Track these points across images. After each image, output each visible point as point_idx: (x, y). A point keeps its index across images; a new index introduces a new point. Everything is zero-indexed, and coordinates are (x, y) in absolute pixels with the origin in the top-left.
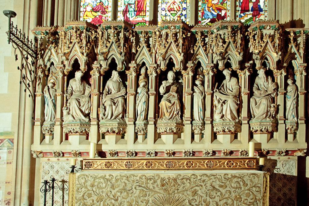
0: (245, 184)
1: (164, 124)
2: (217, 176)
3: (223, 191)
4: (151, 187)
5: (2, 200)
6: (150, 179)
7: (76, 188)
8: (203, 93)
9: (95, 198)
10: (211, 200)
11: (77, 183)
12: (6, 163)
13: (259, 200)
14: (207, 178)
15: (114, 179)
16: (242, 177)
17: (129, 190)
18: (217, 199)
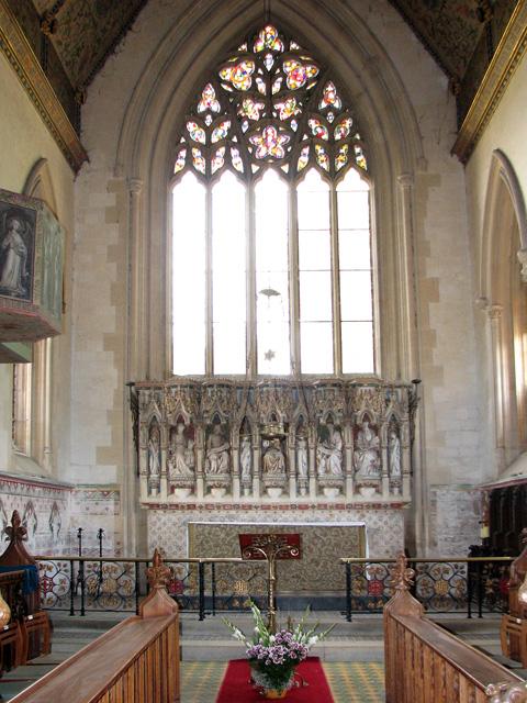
3: (325, 539)
8: (307, 448)
18: (319, 546)
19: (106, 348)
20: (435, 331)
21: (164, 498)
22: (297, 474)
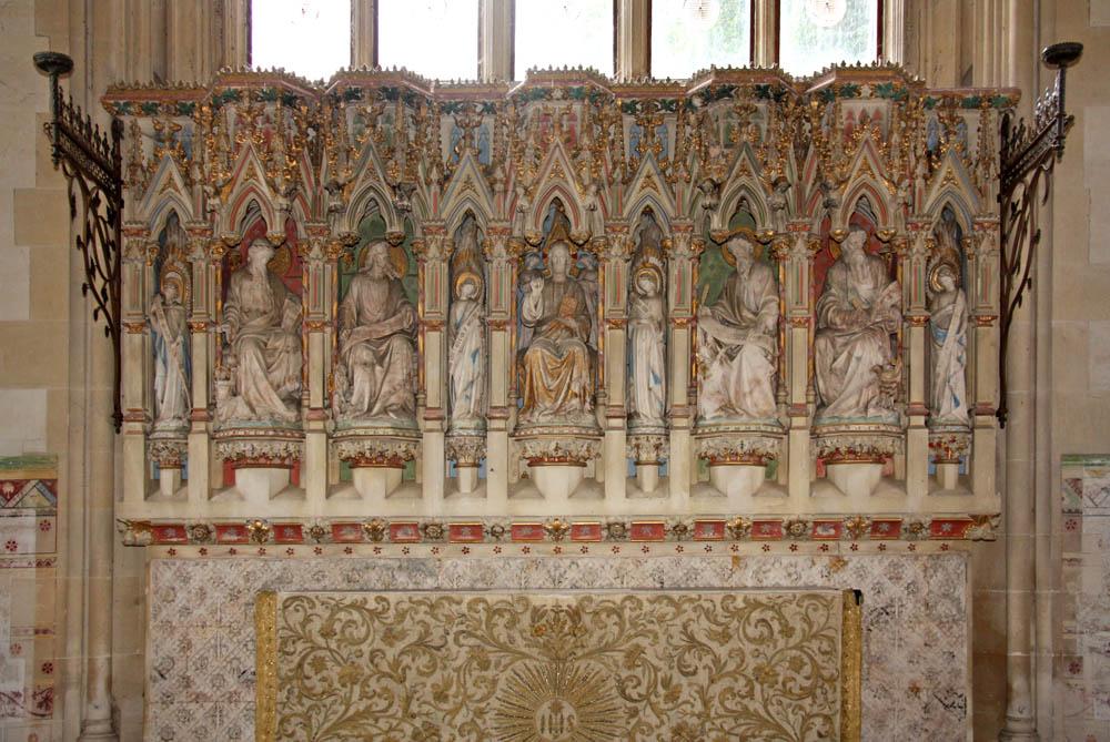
0: (787, 631)
2: (702, 602)
3: (722, 651)
4: (503, 639)
5: (25, 690)
6: (499, 612)
7: (279, 641)
9: (333, 672)
10: (684, 681)
11: (281, 623)
12: (34, 565)
13: (832, 680)
14: (672, 610)
15: (392, 612)
16: (776, 607)
17: (438, 649)
18: (703, 677)
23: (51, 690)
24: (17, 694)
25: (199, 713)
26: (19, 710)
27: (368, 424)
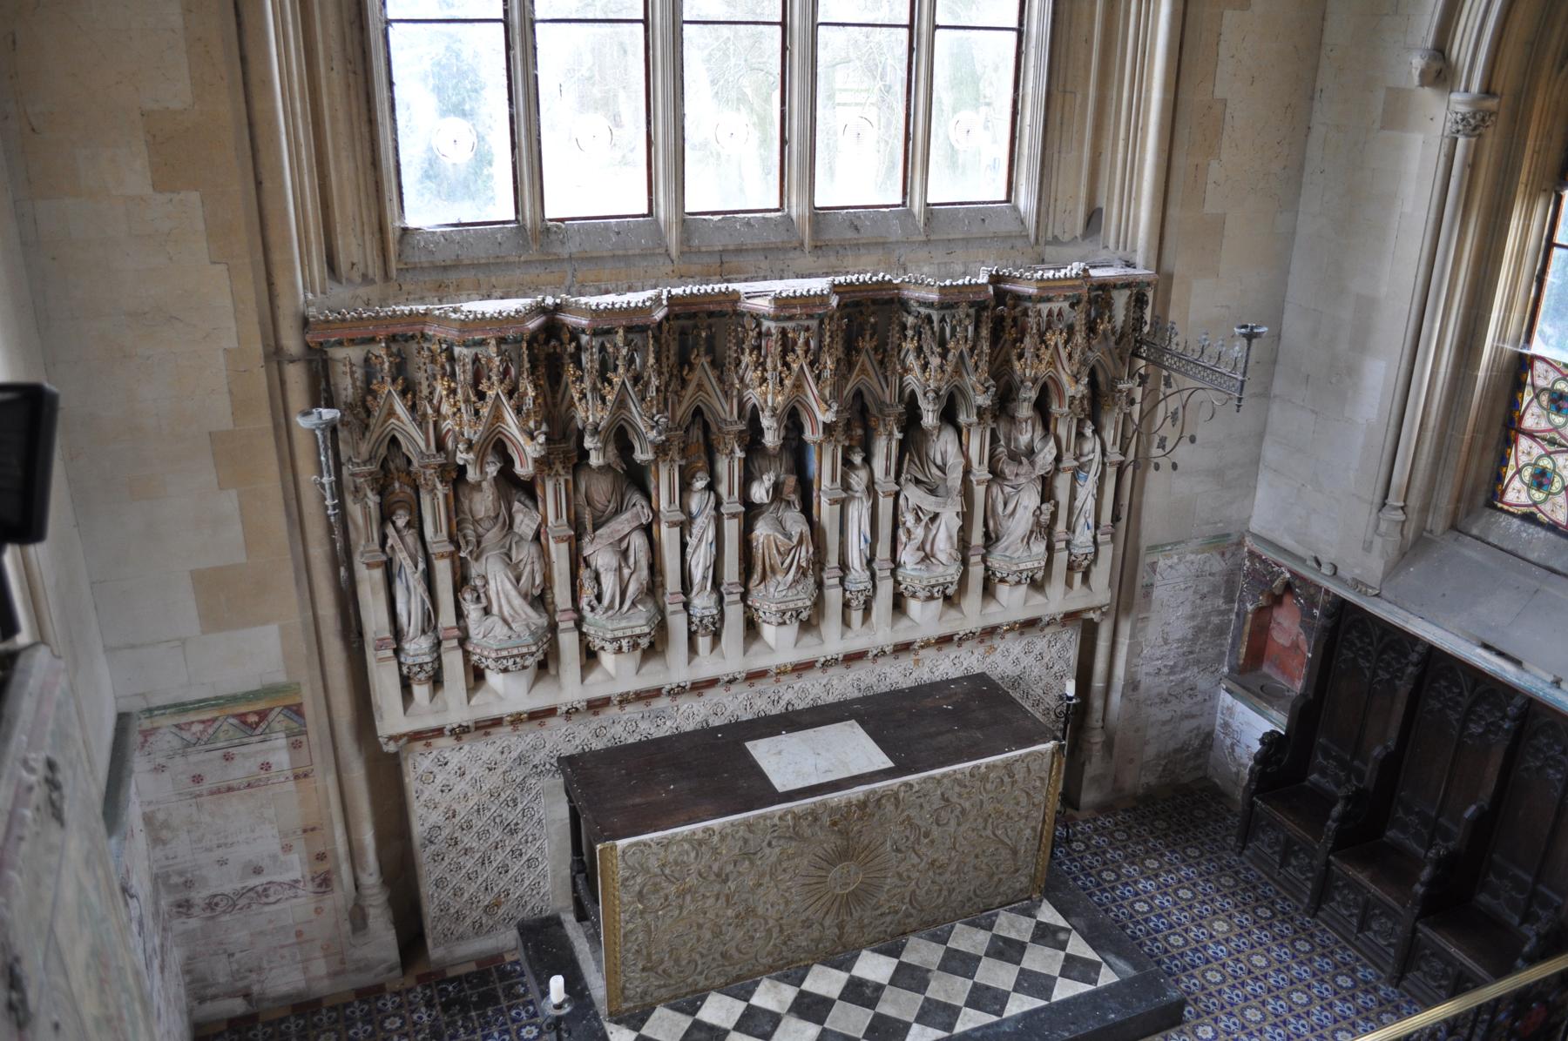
1: (772, 596)
19: (166, 178)
20: (1224, 102)
21: (455, 706)
22: (844, 566)
23: (328, 872)
24: (297, 881)
25: (469, 864)
26: (300, 892)
27: (624, 624)
